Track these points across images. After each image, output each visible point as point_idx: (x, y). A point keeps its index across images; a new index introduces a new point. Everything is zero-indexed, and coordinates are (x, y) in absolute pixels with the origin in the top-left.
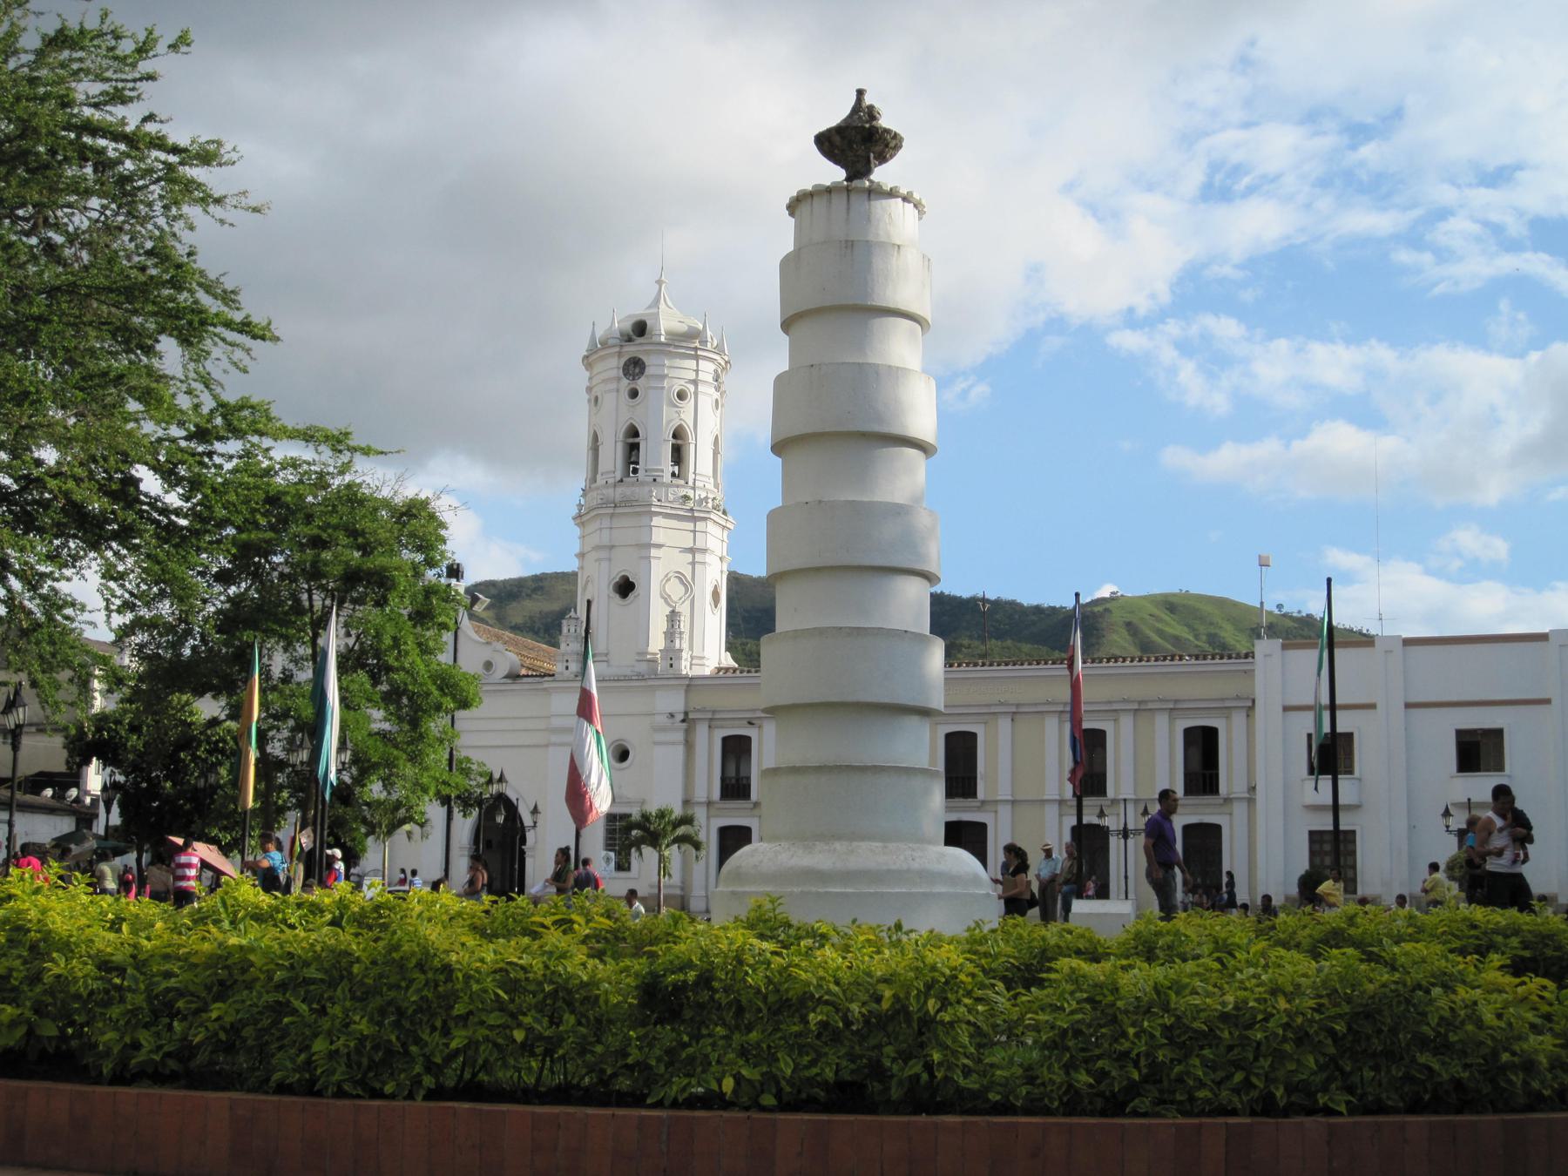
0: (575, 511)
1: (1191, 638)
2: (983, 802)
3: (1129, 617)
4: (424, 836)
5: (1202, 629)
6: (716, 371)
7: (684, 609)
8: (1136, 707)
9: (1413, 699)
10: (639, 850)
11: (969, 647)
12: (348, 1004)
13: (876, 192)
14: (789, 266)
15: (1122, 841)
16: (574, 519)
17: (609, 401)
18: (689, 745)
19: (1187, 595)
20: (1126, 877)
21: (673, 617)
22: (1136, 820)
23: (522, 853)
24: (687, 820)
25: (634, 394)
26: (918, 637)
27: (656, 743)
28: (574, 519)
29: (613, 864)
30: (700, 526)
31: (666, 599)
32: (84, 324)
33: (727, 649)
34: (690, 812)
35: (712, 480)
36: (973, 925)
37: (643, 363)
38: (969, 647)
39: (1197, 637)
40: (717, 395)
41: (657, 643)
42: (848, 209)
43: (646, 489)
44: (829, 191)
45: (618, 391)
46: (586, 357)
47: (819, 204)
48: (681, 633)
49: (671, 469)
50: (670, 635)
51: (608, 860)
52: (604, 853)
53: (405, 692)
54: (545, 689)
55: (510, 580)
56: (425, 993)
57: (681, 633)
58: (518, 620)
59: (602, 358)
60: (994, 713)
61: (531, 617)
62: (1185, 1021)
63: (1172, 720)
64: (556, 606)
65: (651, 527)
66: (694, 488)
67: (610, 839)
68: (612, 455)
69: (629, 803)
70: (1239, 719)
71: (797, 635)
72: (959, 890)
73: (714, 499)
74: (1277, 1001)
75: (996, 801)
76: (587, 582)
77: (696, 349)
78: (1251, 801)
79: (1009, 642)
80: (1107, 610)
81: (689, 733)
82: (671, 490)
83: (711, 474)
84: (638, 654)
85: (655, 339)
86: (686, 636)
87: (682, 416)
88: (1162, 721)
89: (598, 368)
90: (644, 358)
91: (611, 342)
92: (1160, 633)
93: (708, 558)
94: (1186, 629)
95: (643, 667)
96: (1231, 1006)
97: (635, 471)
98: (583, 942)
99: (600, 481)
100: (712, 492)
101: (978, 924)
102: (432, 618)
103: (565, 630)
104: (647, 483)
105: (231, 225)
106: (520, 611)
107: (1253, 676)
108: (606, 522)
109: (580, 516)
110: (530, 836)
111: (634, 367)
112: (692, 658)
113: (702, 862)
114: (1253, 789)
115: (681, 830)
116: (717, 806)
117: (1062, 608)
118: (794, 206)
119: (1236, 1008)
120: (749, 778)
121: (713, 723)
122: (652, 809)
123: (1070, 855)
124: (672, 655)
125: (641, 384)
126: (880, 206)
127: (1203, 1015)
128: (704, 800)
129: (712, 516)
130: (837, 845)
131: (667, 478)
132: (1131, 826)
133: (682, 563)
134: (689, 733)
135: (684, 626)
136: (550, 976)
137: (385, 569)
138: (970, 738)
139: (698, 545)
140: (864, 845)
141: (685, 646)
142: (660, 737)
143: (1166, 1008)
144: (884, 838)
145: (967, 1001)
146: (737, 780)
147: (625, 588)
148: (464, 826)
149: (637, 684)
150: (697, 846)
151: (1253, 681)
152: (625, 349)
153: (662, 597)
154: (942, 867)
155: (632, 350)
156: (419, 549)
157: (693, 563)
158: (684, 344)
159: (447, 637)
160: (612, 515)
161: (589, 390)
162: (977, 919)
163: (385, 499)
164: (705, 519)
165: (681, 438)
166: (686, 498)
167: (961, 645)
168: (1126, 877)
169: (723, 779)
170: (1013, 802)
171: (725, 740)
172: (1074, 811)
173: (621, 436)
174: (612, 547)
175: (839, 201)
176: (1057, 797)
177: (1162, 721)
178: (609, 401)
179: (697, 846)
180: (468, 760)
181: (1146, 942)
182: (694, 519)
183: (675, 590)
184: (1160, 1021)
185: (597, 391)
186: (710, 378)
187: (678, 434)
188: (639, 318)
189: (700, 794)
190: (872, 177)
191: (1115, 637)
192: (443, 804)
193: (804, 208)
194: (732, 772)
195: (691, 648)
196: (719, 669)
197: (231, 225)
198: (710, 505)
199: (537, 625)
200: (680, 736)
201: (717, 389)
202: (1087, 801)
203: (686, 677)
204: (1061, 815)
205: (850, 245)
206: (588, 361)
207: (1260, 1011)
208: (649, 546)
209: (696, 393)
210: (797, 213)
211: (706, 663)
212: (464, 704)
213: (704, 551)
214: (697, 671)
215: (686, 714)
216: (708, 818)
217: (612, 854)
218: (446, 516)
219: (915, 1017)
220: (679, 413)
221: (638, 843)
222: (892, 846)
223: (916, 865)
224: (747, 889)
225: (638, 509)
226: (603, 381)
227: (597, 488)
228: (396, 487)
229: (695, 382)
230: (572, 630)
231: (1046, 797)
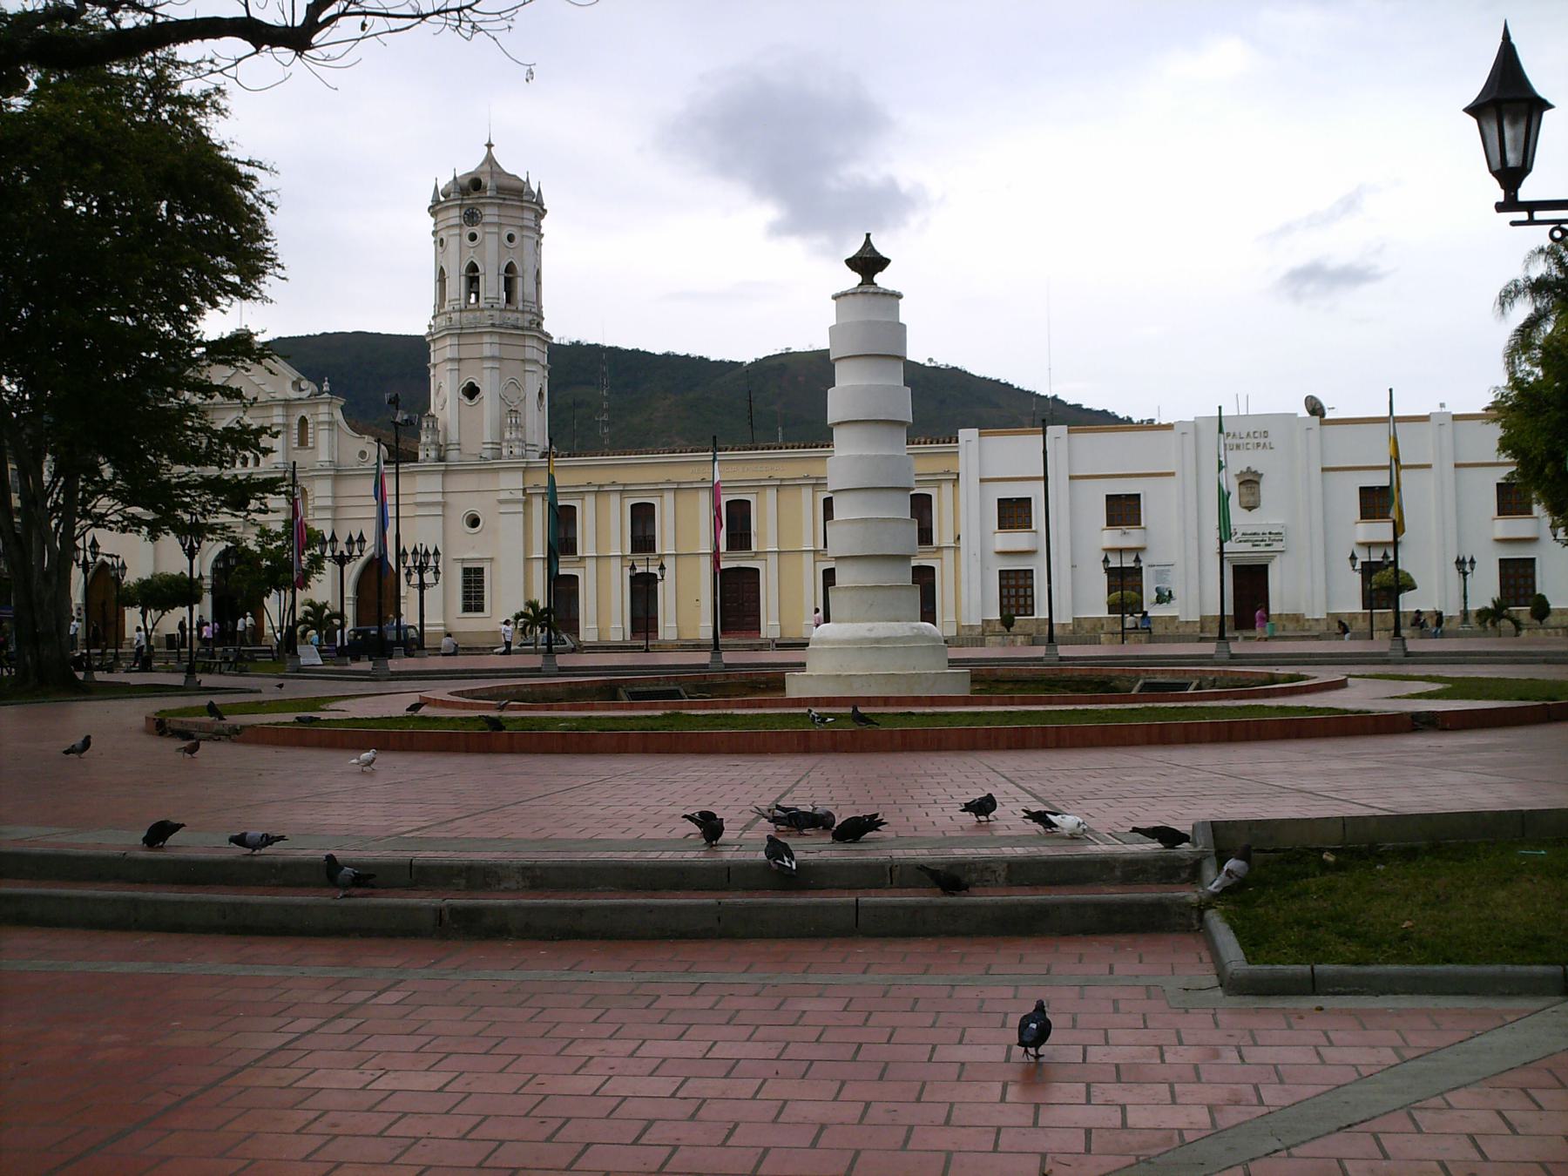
8: (596, 489)
9: (1459, 462)
18: (527, 515)
32: (264, 201)
45: (460, 235)
60: (661, 489)
63: (814, 492)
68: (456, 285)
70: (947, 488)
78: (957, 549)
88: (615, 499)
89: (440, 217)
99: (447, 308)
103: (425, 425)
105: (489, 145)
107: (958, 456)
134: (527, 503)
138: (650, 508)
142: (503, 509)
146: (566, 540)
151: (958, 462)
152: (464, 202)
161: (435, 233)
165: (511, 273)
171: (633, 506)
177: (615, 499)
185: (443, 234)
188: (474, 176)
197: (489, 145)
204: (815, 562)
206: (435, 209)
225: (478, 330)
227: (445, 313)
230: (431, 426)
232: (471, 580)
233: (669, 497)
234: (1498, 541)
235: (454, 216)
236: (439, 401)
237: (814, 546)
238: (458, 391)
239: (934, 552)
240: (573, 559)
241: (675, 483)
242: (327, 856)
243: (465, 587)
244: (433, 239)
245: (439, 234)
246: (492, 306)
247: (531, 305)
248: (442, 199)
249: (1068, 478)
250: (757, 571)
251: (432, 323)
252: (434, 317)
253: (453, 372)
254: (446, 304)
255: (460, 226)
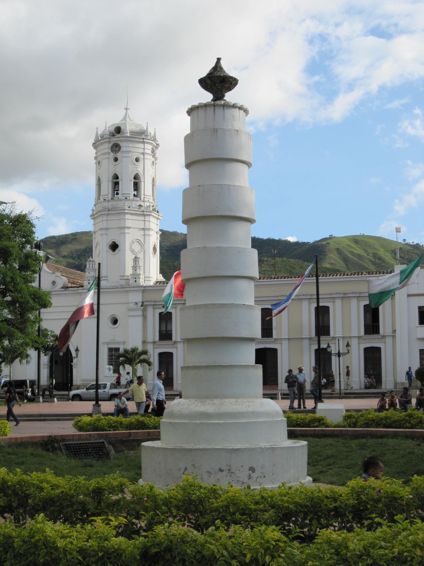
0: (91, 213)
1: (366, 255)
2: (276, 339)
3: (337, 246)
4: (28, 362)
5: (370, 251)
6: (152, 148)
7: (141, 256)
8: (342, 296)
10: (124, 366)
11: (267, 261)
12: (13, 561)
13: (227, 106)
14: (188, 139)
15: (338, 358)
16: (91, 216)
17: (105, 163)
18: (144, 316)
19: (363, 236)
20: (340, 374)
21: (136, 259)
22: (343, 349)
23: (72, 366)
24: (145, 352)
25: (116, 160)
26: (250, 307)
27: (129, 316)
28: (91, 216)
29: (112, 371)
30: (147, 218)
31: (133, 251)
33: (160, 273)
34: (146, 349)
35: (152, 198)
36: (281, 485)
37: (120, 146)
38: (267, 261)
39: (368, 254)
40: (153, 159)
41: (129, 271)
42: (214, 114)
43: (123, 202)
44: (206, 106)
46: (94, 144)
47: (201, 112)
48: (139, 267)
49: (133, 193)
50: (135, 268)
51: (110, 369)
52: (108, 366)
53: (18, 301)
54: (80, 293)
55: (62, 235)
56: (46, 558)
57: (139, 267)
58: (65, 253)
59: (101, 144)
61: (71, 252)
62: (376, 561)
63: (358, 301)
64: (82, 247)
65: (125, 219)
66: (144, 201)
67: (110, 359)
69: (118, 343)
71: (195, 307)
72: (270, 419)
73: (153, 206)
74: (416, 551)
75: (282, 339)
76: (97, 244)
77: (143, 139)
78: (394, 337)
79: (285, 259)
80: (328, 243)
81: (144, 311)
82: (134, 202)
83: (151, 195)
84: (121, 276)
85: (125, 135)
86: (142, 268)
87: (138, 169)
88: (354, 302)
89: (100, 148)
90: (120, 143)
91: (105, 136)
92: (352, 253)
93: (151, 233)
94: (363, 251)
95: (123, 282)
96: (396, 554)
97: (117, 194)
98: (114, 529)
100: (152, 203)
101: (283, 484)
102: (29, 268)
104: (123, 200)
106: (65, 250)
108: (105, 218)
109: (93, 215)
110: (75, 361)
111: (116, 148)
112: (145, 277)
113: (152, 371)
114: (394, 331)
115: (142, 357)
116: (157, 343)
117: (308, 243)
118: (190, 112)
119: (399, 554)
120: (171, 331)
121: (155, 307)
122: (129, 347)
123: (316, 372)
124: (136, 277)
125: (119, 155)
126: (229, 112)
127: (384, 557)
128: (152, 341)
129: (152, 214)
130: (216, 401)
131: (132, 197)
132: (341, 351)
133: (139, 235)
134: (144, 311)
135: (141, 263)
136: (101, 548)
137: (7, 247)
139: (147, 227)
140: (227, 400)
141: (142, 272)
142: (131, 313)
143: (368, 555)
144: (237, 397)
145: (283, 555)
146: (166, 332)
147: (114, 247)
148: (45, 359)
149: (120, 290)
150: (149, 364)
152: (111, 140)
153: (131, 250)
154: (262, 409)
155: (114, 140)
156: (24, 237)
157: (144, 235)
158: (138, 137)
159: (37, 275)
160: (108, 214)
161: (96, 158)
162: (283, 482)
163: (7, 214)
164: (149, 215)
165: (138, 179)
166: (140, 206)
167: (264, 260)
168: (340, 374)
169: (160, 331)
170: (289, 339)
171: (160, 314)
172: (317, 342)
173: (111, 179)
174: (108, 229)
175: (210, 110)
176: (308, 337)
177: (354, 302)
178: (105, 163)
179: (149, 364)
180: (46, 330)
181: (356, 492)
182: (145, 215)
183: (137, 247)
184: (366, 562)
185: (100, 158)
186: (150, 152)
187: (136, 177)
189: (150, 339)
190: (225, 98)
191: (332, 255)
192: (36, 350)
193: (195, 113)
194: (164, 328)
195: (144, 273)
196: (157, 282)
198: (151, 209)
199: (74, 255)
200: (140, 313)
201: (153, 156)
202: (322, 338)
203: (142, 286)
204: (310, 345)
205: (215, 130)
206: (95, 145)
207: (409, 556)
208: (124, 228)
209: (144, 159)
210: (192, 114)
211: (150, 279)
212: (45, 306)
213: (149, 229)
214: (147, 284)
215: (143, 302)
216: (154, 349)
217: (111, 367)
218: (35, 222)
219: (261, 564)
220: (136, 168)
221: (123, 363)
222: (240, 400)
223: (250, 409)
224: (176, 421)
225: (118, 212)
226: (102, 154)
227: (101, 203)
228: (12, 209)
229: (143, 154)
230: (91, 266)
231: (303, 337)
232: (112, 355)
233: (338, 302)
234: (418, 339)
235: (106, 147)
236: (97, 252)
237: (343, 334)
238: (107, 246)
239: (380, 339)
240: (271, 340)
241: (342, 293)
242: (350, 532)
243: (109, 359)
244: (95, 161)
245: (98, 158)
246: (126, 198)
247: (149, 197)
248: (100, 138)
249: (406, 295)
250: (275, 350)
251: (94, 209)
252: (95, 205)
253: (104, 236)
254: (101, 197)
255: (109, 153)
